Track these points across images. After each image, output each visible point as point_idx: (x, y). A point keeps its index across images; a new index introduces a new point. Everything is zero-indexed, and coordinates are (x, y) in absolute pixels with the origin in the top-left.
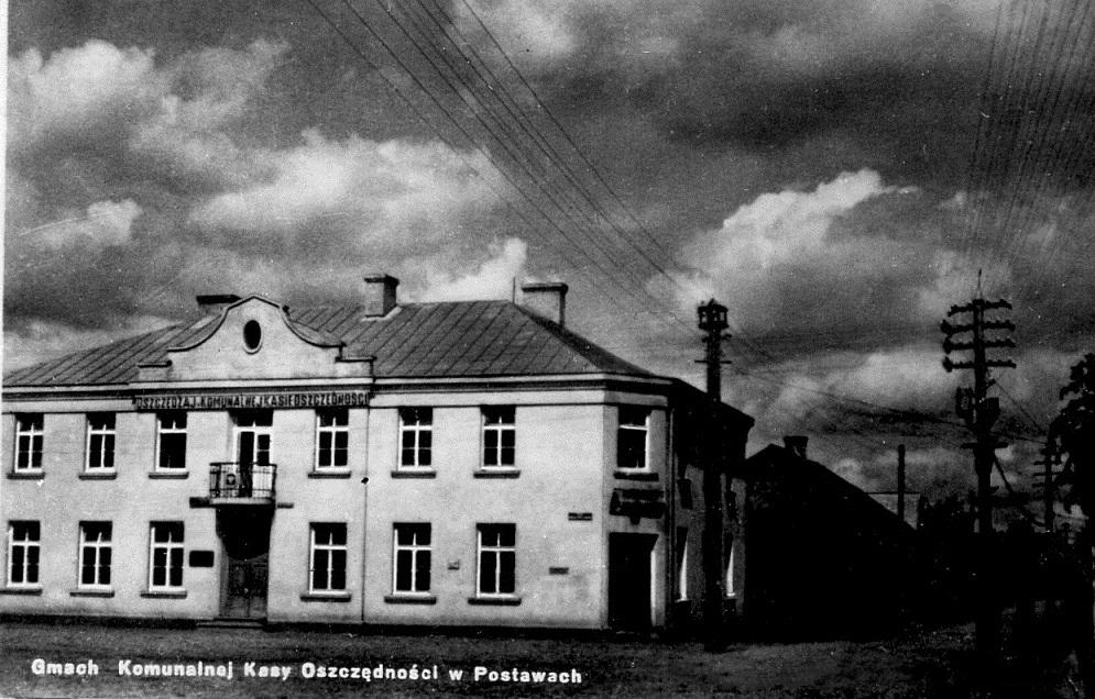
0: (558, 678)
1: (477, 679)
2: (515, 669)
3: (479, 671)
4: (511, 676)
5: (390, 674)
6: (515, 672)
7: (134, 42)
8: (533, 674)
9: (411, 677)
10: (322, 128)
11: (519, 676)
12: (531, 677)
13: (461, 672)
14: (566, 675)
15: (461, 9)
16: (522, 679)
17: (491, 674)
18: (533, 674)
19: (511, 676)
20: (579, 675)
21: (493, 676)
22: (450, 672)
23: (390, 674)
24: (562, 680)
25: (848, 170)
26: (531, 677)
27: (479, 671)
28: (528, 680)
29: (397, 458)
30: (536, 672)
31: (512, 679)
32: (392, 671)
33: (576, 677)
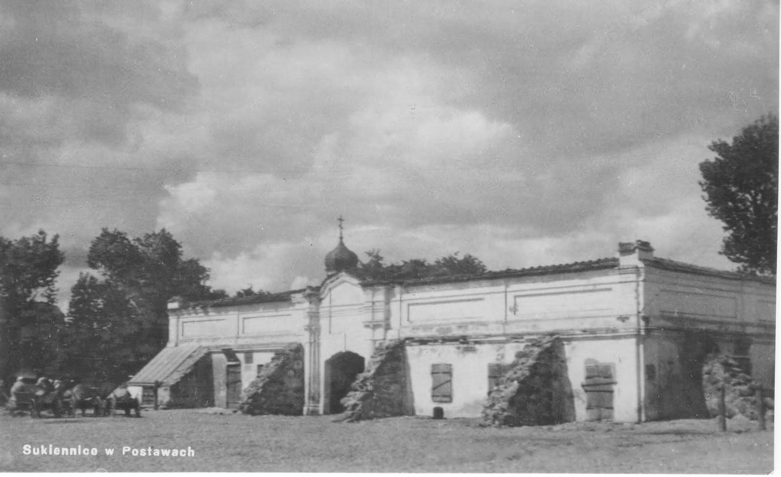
0: (179, 453)
1: (124, 453)
2: (150, 448)
3: (126, 449)
4: (147, 452)
5: (36, 451)
6: (150, 450)
7: (266, 296)
8: (162, 450)
9: (141, 454)
10: (484, 270)
11: (152, 453)
12: (161, 452)
13: (113, 450)
14: (184, 451)
15: (1, 385)
16: (173, 455)
17: (137, 452)
18: (162, 450)
19: (147, 452)
20: (193, 451)
21: (135, 452)
22: (106, 450)
23: (36, 451)
24: (181, 455)
25: (398, 345)
26: (161, 452)
27: (126, 449)
28: (158, 454)
29: (471, 318)
30: (108, 449)
31: (48, 453)
32: (67, 450)
33: (191, 452)
